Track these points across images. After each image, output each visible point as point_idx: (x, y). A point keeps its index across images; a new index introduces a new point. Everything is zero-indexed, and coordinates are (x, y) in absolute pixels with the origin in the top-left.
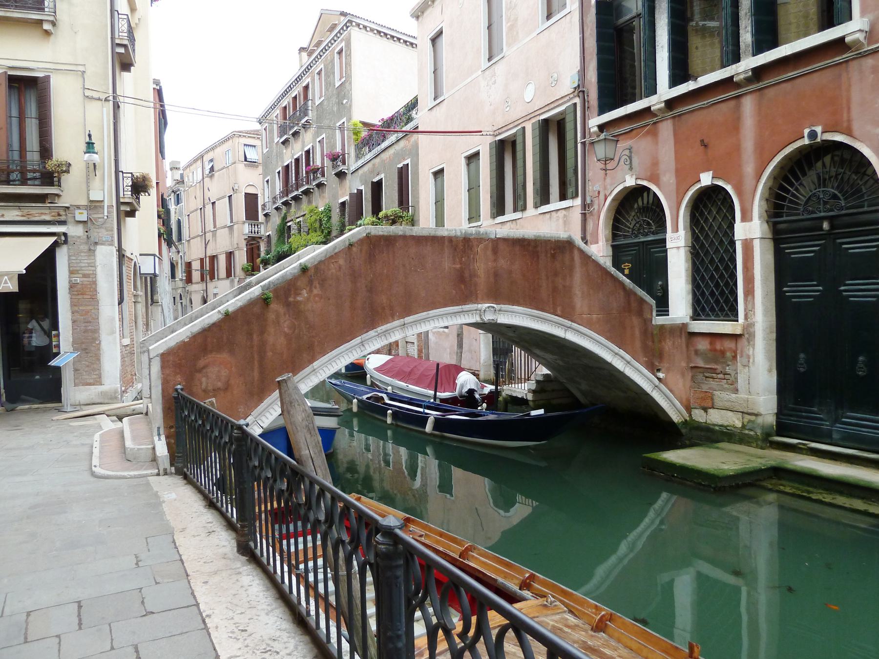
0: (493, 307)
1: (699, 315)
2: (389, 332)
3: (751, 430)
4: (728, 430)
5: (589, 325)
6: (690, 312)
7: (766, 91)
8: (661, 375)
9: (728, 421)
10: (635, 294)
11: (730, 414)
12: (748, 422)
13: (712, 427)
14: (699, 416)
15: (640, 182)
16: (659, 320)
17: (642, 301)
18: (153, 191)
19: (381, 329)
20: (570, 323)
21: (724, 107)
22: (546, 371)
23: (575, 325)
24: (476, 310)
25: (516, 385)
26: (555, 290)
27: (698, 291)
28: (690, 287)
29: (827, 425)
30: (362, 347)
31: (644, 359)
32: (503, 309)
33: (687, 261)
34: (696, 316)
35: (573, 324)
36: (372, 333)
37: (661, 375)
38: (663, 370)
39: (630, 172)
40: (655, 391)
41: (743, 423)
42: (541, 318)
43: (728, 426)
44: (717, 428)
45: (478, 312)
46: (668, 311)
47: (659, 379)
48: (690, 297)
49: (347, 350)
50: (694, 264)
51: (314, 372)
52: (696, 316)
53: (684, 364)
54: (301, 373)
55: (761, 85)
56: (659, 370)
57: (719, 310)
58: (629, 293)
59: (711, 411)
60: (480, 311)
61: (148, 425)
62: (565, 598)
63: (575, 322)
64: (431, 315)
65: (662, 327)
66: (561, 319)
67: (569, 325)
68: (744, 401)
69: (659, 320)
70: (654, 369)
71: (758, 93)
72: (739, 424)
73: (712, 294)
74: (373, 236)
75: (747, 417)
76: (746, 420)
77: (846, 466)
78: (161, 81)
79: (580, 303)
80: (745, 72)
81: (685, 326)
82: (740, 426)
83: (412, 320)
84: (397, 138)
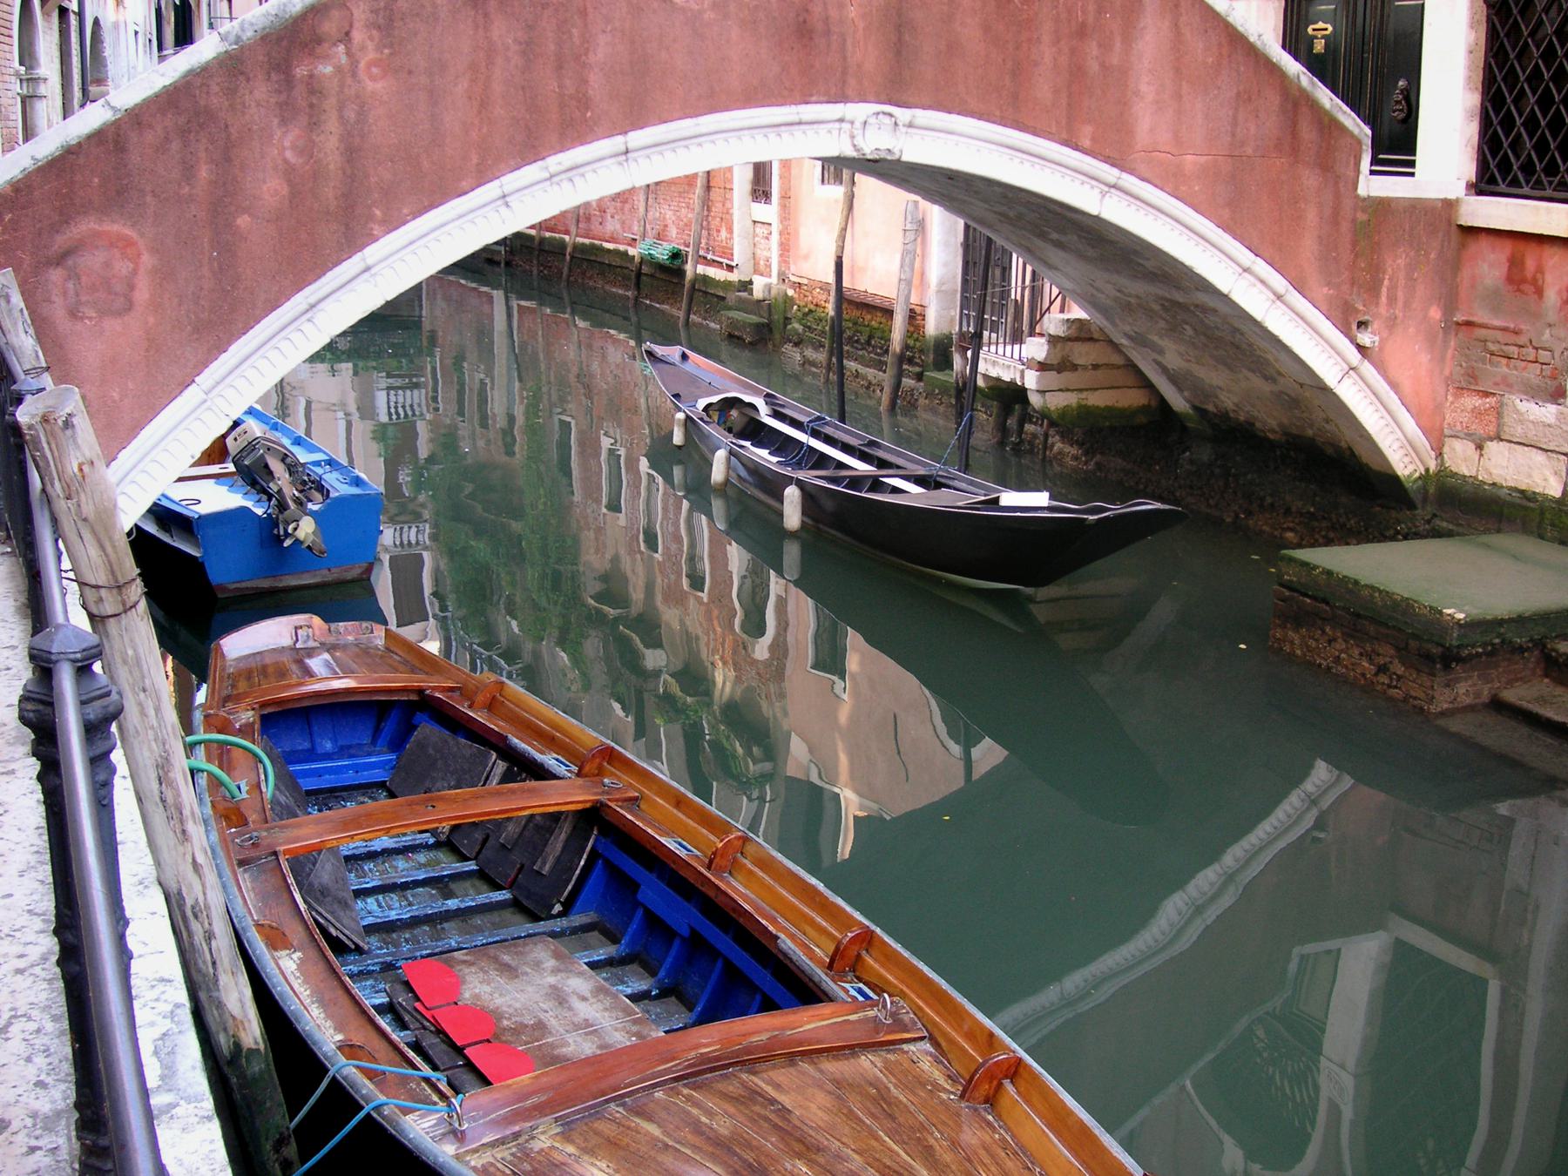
0: (891, 115)
1: (1492, 181)
2: (581, 170)
5: (1172, 182)
6: (1469, 170)
8: (1365, 338)
9: (1530, 476)
10: (1314, 105)
11: (1539, 457)
14: (1462, 460)
16: (1374, 186)
17: (1329, 126)
19: (557, 161)
20: (1115, 172)
22: (1077, 312)
23: (1129, 181)
24: (841, 120)
25: (1009, 348)
26: (1077, 72)
27: (1497, 113)
28: (1474, 99)
30: (503, 210)
31: (1325, 290)
32: (918, 122)
33: (1473, 25)
34: (1485, 184)
35: (1125, 176)
36: (531, 172)
37: (1365, 338)
38: (1375, 325)
40: (1347, 382)
42: (1031, 155)
45: (846, 126)
46: (1412, 164)
47: (1361, 349)
48: (1473, 129)
49: (461, 216)
50: (1492, 35)
51: (366, 275)
52: (1485, 184)
53: (1435, 313)
54: (330, 275)
56: (1362, 325)
57: (1542, 170)
58: (1297, 102)
59: (1492, 447)
60: (852, 123)
61: (1076, 369)
62: (888, 970)
63: (1132, 172)
64: (704, 130)
65: (1382, 206)
66: (1088, 159)
67: (1112, 180)
69: (1374, 186)
70: (1349, 321)
73: (1531, 124)
77: (126, 1104)
79: (1148, 123)
81: (1450, 205)
83: (650, 141)
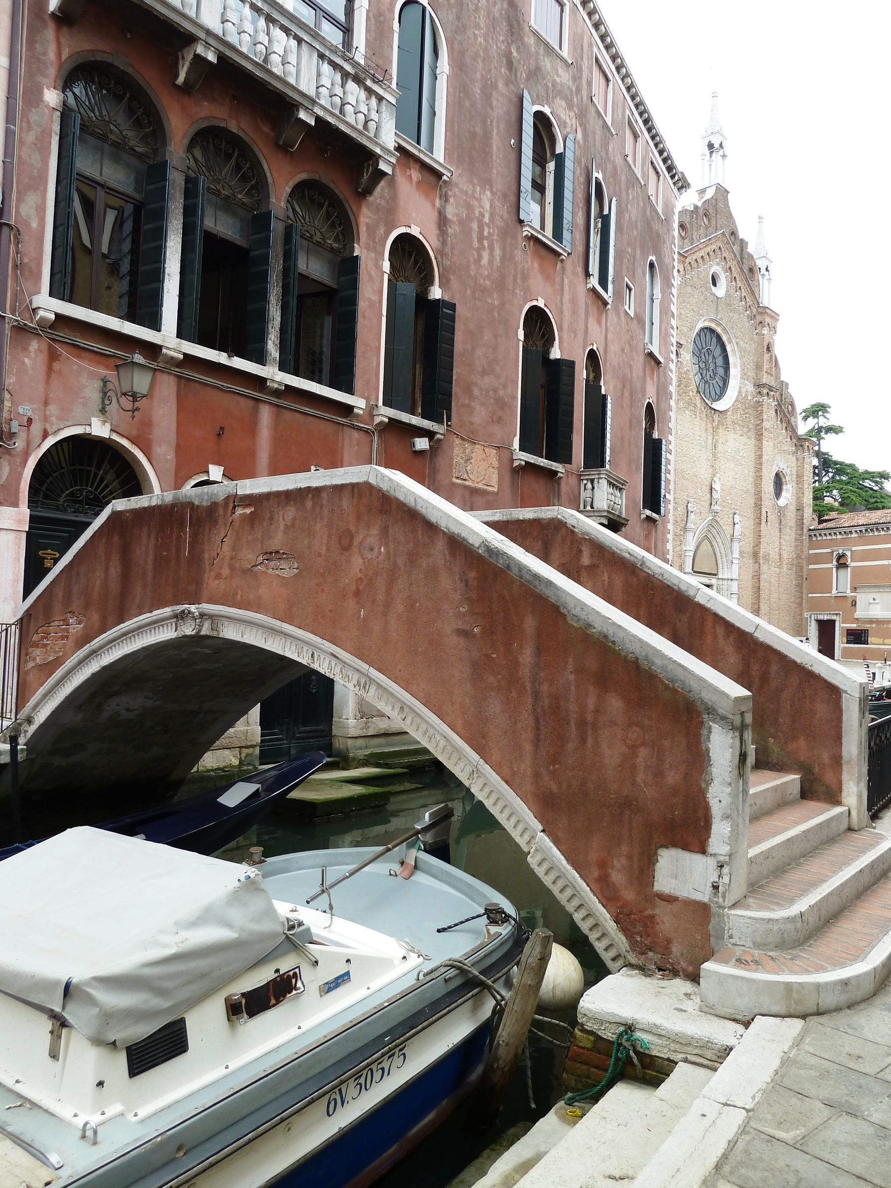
3: (249, 764)
4: (226, 771)
7: (284, 411)
9: (224, 761)
12: (246, 757)
13: (206, 774)
15: (115, 437)
18: (495, 267)
21: (243, 402)
29: (286, 744)
39: (101, 416)
41: (240, 759)
43: (225, 767)
44: (212, 773)
55: (281, 402)
68: (243, 733)
71: (275, 409)
72: (236, 762)
74: (695, 602)
75: (245, 751)
76: (243, 755)
78: (780, 318)
80: (280, 383)
82: (238, 763)
84: (766, 557)
